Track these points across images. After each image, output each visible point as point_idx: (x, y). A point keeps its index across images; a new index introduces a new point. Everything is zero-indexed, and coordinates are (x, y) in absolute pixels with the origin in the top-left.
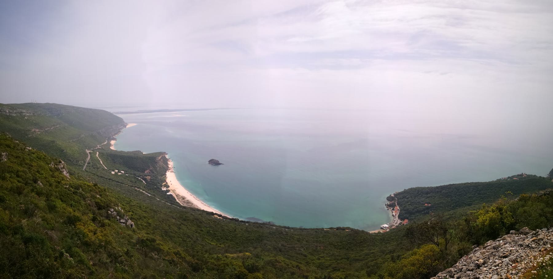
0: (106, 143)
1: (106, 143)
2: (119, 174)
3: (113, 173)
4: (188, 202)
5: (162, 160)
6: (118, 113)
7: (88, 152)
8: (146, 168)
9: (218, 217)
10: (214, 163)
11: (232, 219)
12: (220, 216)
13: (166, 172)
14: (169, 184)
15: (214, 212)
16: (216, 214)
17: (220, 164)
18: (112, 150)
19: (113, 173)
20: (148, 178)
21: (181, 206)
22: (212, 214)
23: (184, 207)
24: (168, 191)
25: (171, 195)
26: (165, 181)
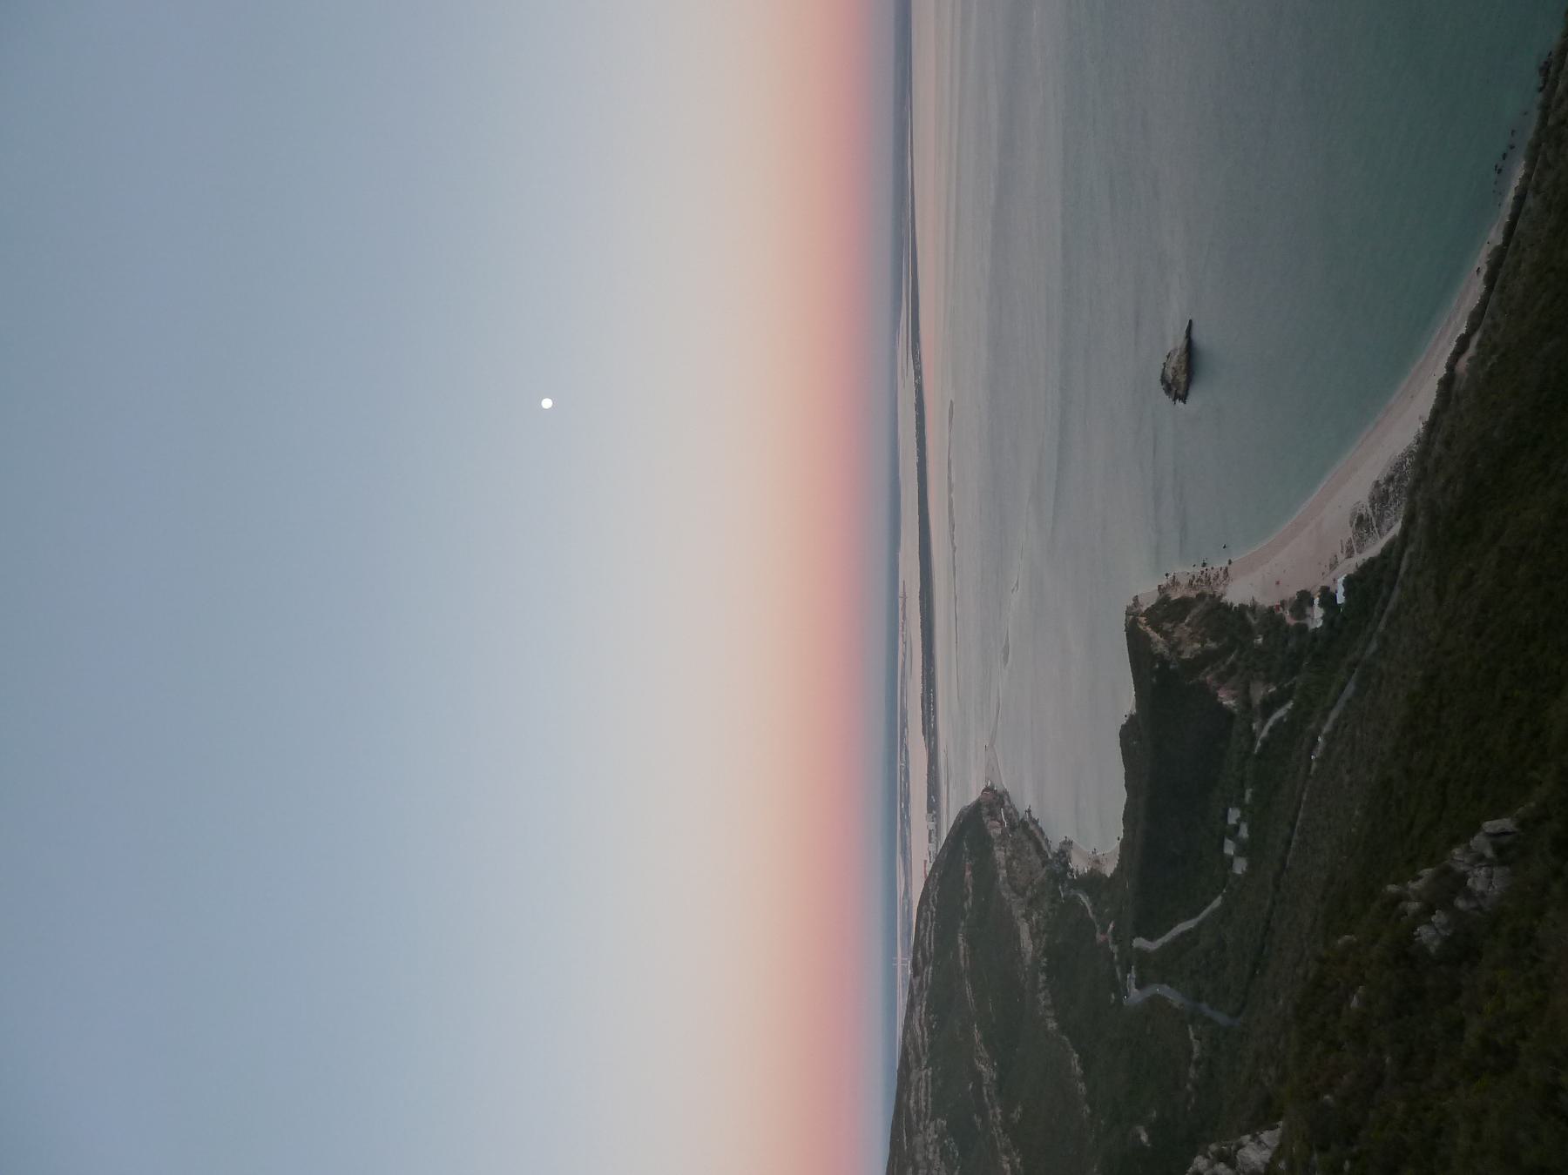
0: (1085, 899)
1: (1085, 899)
2: (1244, 832)
3: (1240, 866)
4: (1381, 498)
5: (1167, 626)
6: (933, 834)
7: (1135, 995)
8: (1198, 687)
9: (1471, 351)
10: (1183, 374)
11: (1490, 280)
12: (1463, 343)
13: (1227, 608)
14: (1291, 593)
15: (1441, 371)
16: (1451, 367)
17: (1190, 348)
18: (1120, 869)
19: (1240, 866)
20: (1259, 693)
21: (1405, 533)
22: (1447, 383)
23: (1410, 520)
24: (1328, 597)
25: (1349, 582)
26: (1271, 610)
